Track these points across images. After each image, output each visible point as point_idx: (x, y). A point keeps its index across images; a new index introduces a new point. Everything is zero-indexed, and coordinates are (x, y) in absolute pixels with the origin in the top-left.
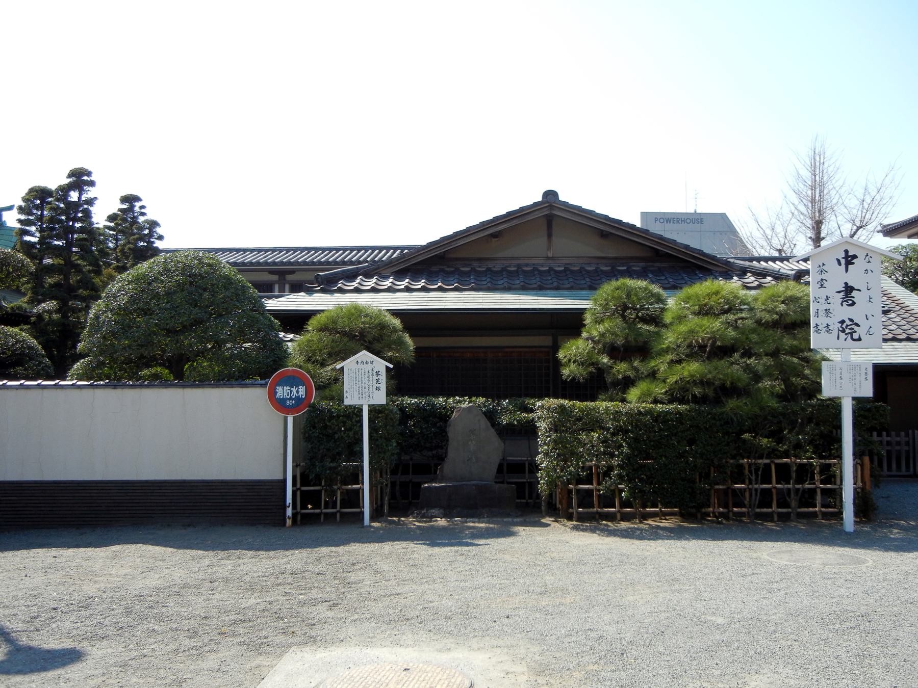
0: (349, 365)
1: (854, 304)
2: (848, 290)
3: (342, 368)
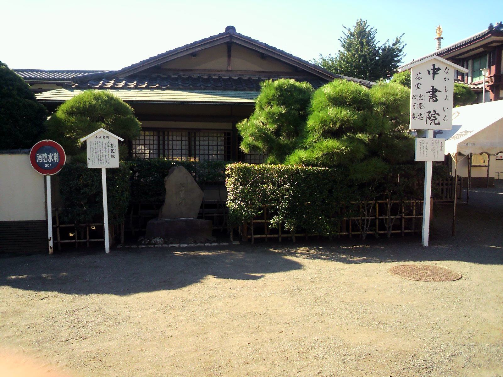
0: (90, 139)
1: (436, 100)
2: (434, 91)
3: (85, 142)
